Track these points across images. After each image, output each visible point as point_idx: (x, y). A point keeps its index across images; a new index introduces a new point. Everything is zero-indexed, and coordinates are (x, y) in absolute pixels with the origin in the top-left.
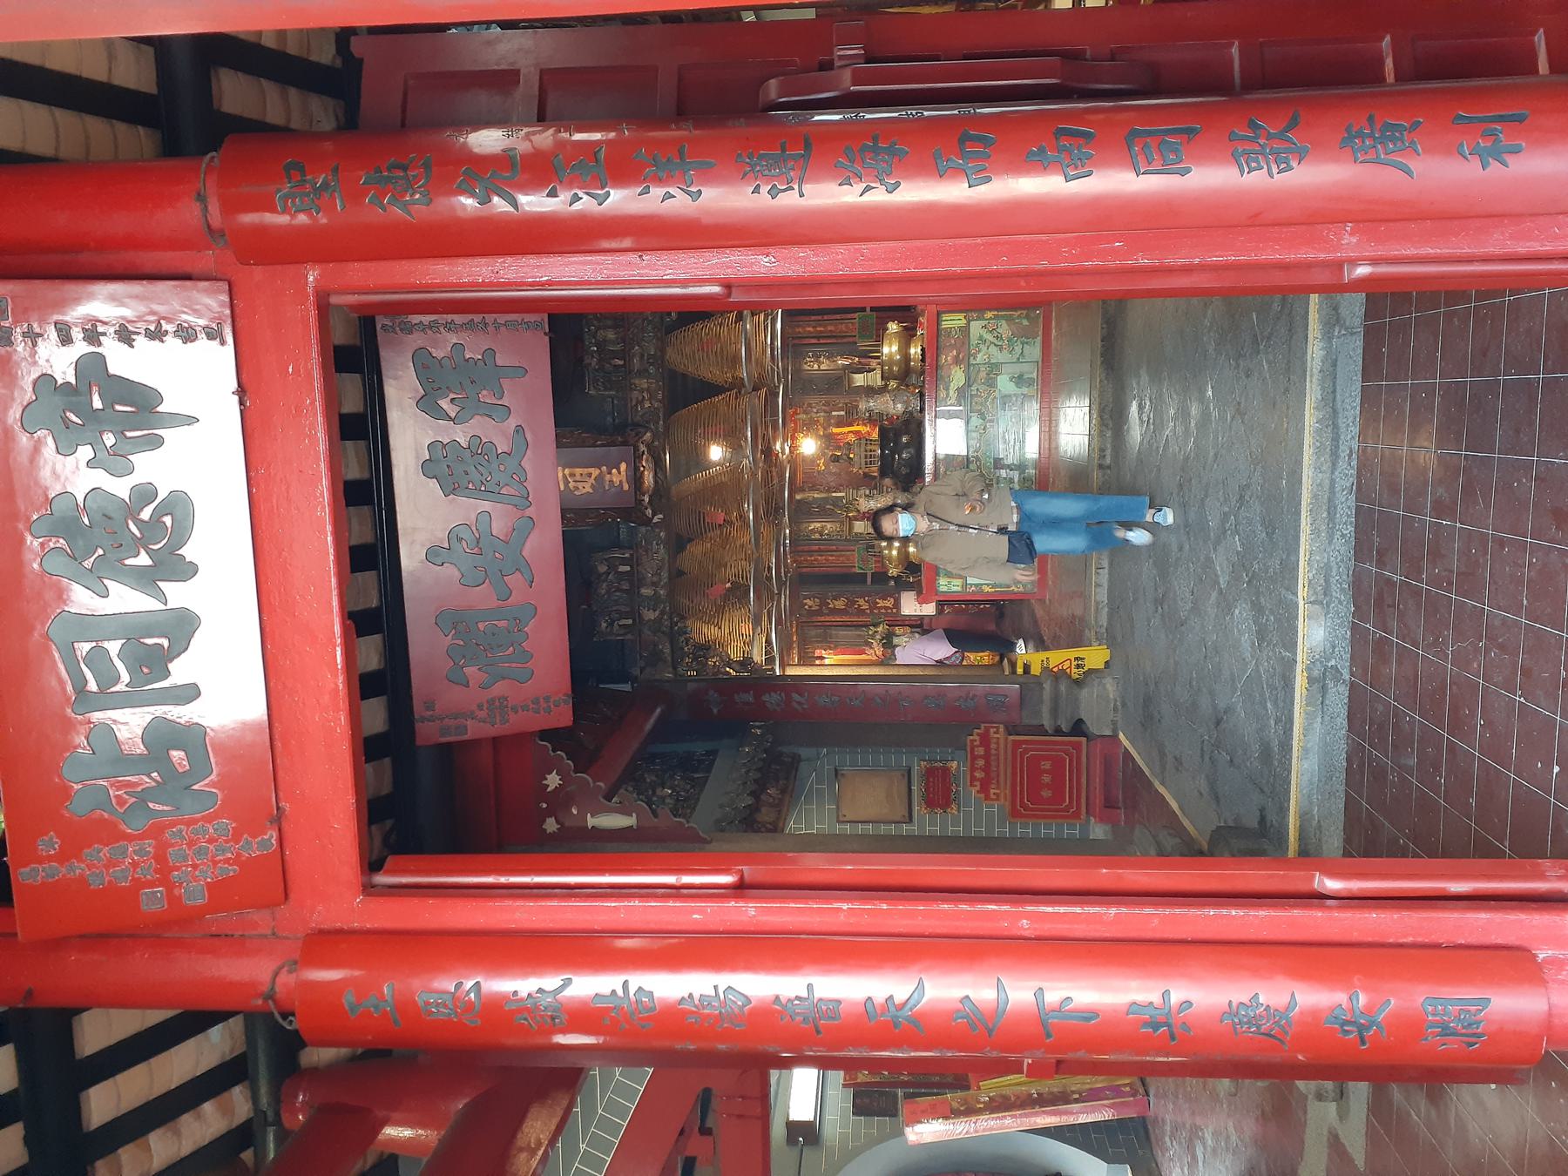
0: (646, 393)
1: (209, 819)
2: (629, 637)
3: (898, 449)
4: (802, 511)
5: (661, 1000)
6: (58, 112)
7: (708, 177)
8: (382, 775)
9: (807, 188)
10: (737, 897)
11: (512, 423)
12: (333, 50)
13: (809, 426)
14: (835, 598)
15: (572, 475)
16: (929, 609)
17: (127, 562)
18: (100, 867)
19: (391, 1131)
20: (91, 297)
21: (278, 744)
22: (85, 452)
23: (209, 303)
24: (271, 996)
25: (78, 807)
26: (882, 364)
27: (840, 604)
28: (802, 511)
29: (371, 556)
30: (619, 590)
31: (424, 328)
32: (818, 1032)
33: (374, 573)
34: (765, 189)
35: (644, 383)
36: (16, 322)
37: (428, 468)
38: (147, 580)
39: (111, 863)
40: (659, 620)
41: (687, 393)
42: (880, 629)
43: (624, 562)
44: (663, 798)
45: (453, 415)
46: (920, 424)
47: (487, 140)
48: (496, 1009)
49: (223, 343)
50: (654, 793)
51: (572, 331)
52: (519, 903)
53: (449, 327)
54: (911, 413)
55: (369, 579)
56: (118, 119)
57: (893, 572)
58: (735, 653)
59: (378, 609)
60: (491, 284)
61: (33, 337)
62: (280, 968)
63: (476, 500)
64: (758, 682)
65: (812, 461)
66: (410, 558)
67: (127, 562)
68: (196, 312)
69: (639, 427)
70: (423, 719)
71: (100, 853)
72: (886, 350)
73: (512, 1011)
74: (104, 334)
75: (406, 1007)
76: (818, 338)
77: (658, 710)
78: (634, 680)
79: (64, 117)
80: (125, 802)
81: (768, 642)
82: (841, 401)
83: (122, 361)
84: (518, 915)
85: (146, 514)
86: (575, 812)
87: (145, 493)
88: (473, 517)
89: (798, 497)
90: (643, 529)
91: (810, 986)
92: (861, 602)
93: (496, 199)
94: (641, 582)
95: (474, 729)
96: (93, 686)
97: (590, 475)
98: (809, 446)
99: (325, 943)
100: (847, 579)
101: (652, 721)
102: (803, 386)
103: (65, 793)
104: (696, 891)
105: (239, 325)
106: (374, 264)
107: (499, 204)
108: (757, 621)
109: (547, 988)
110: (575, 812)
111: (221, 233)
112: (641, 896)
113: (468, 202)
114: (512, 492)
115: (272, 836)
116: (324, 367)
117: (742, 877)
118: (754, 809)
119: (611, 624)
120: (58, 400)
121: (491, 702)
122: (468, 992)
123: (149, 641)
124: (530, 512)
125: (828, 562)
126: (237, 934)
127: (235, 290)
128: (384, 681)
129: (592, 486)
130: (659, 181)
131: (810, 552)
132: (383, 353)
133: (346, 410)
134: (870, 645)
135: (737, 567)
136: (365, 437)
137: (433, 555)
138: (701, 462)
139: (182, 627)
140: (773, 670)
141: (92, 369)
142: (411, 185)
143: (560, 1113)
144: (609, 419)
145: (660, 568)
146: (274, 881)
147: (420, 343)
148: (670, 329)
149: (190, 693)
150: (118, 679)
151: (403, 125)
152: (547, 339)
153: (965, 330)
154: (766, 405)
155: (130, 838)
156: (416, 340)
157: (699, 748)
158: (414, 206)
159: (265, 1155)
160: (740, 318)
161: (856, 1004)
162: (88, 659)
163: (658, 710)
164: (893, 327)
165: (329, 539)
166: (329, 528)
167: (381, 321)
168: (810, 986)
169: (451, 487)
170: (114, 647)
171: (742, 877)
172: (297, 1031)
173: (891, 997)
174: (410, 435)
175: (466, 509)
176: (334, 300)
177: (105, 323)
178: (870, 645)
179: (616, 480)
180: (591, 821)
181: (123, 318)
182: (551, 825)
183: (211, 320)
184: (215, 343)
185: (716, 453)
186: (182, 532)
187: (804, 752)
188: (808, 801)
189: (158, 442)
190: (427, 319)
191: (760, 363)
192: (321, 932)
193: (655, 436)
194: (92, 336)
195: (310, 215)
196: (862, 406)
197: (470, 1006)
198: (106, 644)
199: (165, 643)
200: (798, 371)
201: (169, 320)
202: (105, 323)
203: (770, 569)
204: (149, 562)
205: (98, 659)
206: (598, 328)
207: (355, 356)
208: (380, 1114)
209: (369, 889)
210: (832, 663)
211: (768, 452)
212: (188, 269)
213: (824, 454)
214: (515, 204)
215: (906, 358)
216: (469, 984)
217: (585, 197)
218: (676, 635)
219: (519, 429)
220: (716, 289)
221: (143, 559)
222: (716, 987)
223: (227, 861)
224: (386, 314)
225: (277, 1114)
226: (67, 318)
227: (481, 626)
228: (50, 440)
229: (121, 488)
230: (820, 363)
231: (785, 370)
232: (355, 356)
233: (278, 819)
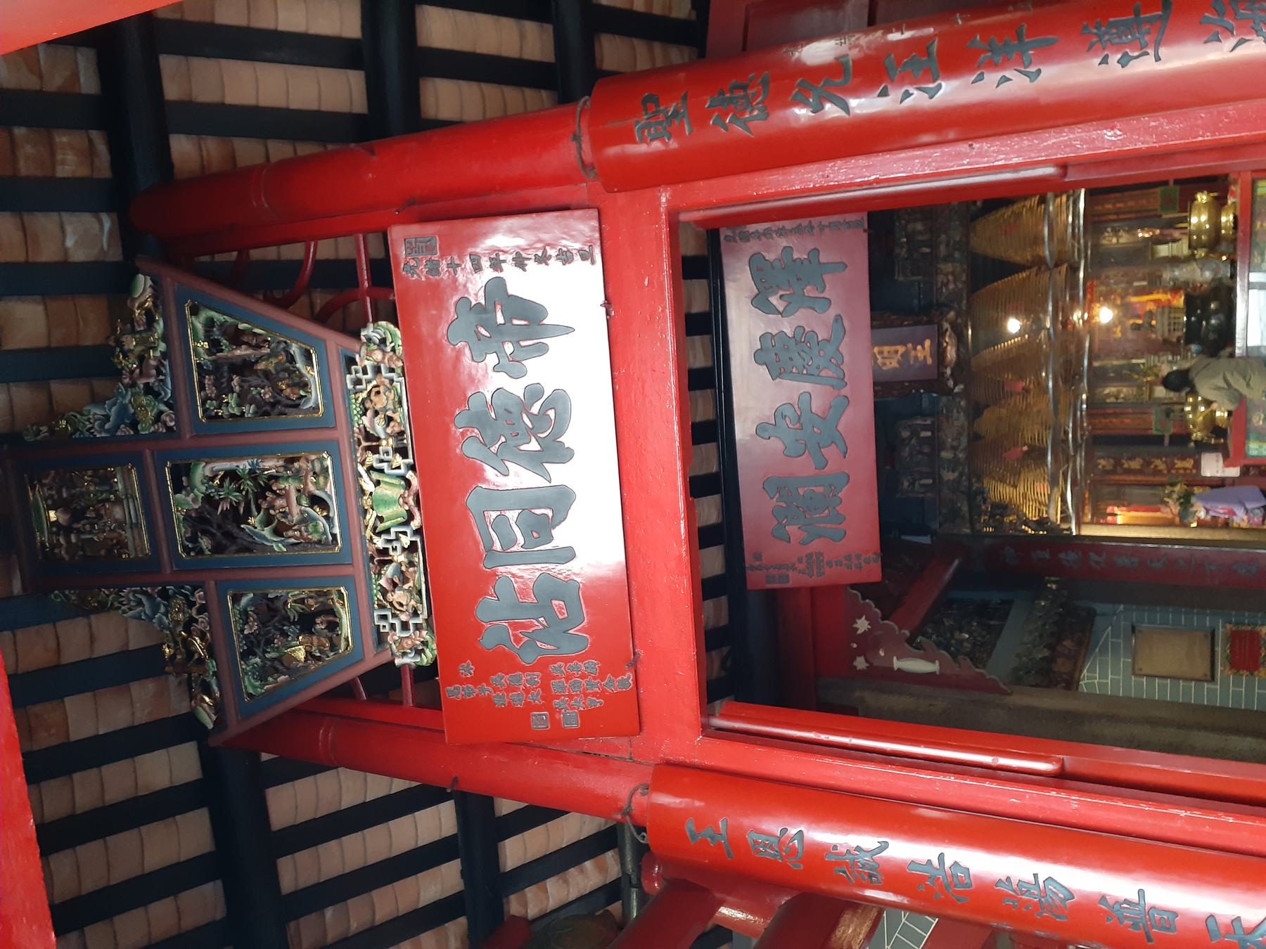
0: (950, 278)
1: (581, 658)
2: (929, 495)
3: (1207, 315)
4: (1099, 377)
5: (978, 878)
6: (485, 86)
7: (1049, 54)
8: (716, 611)
9: (1163, 51)
10: (1059, 788)
11: (832, 313)
12: (689, 6)
13: (1107, 298)
14: (1130, 459)
15: (881, 353)
16: (1234, 472)
17: (523, 447)
18: (505, 691)
19: (725, 911)
20: (495, 231)
21: (634, 599)
22: (492, 359)
23: (579, 230)
24: (628, 813)
25: (488, 641)
26: (1190, 235)
27: (1135, 464)
28: (1099, 377)
29: (710, 429)
30: (920, 452)
31: (758, 235)
32: (1149, 940)
33: (714, 444)
34: (1114, 58)
35: (948, 267)
36: (443, 256)
37: (759, 357)
38: (536, 462)
39: (510, 689)
40: (958, 481)
41: (991, 276)
42: (1177, 488)
43: (925, 428)
44: (961, 642)
45: (781, 309)
46: (1231, 291)
47: (818, 52)
48: (817, 854)
49: (593, 262)
50: (952, 636)
51: (892, 229)
52: (839, 762)
53: (781, 232)
54: (1220, 279)
55: (710, 450)
56: (527, 86)
57: (1197, 435)
58: (1032, 515)
59: (716, 475)
60: (821, 188)
61: (453, 266)
62: (635, 790)
63: (800, 373)
64: (1057, 541)
65: (1108, 329)
66: (743, 430)
67: (523, 447)
68: (573, 238)
69: (943, 307)
70: (753, 568)
71: (501, 679)
72: (1194, 220)
73: (831, 863)
74: (504, 261)
75: (738, 841)
77: (956, 562)
78: (933, 533)
79: (491, 90)
80: (521, 639)
81: (1064, 501)
82: (1141, 271)
83: (520, 283)
84: (837, 773)
85: (535, 409)
86: (882, 653)
87: (534, 392)
88: (796, 397)
89: (1096, 364)
90: (944, 399)
91: (1141, 893)
92: (1158, 462)
93: (828, 106)
94: (942, 446)
95: (795, 579)
96: (498, 546)
97: (897, 352)
99: (672, 773)
100: (1145, 441)
101: (951, 570)
102: (1100, 260)
103: (478, 629)
104: (1013, 773)
105: (607, 245)
106: (713, 182)
107: (831, 111)
108: (1054, 482)
109: (864, 846)
110: (882, 653)
111: (592, 166)
112: (955, 773)
113: (802, 113)
114: (830, 374)
115: (629, 677)
116: (673, 277)
117: (1063, 766)
118: (1050, 660)
119: (912, 484)
120: (473, 318)
121: (809, 556)
122: (792, 839)
123: (538, 512)
124: (845, 391)
125: (1128, 424)
126: (603, 754)
127: (603, 216)
128: (720, 534)
129: (899, 362)
130: (992, 65)
131: (1105, 415)
132: (725, 260)
133: (695, 310)
134: (1166, 504)
135: (1032, 431)
136: (709, 332)
137: (762, 430)
138: (1002, 336)
139: (562, 500)
140: (1070, 529)
141: (497, 289)
142: (750, 104)
143: (869, 923)
144: (916, 301)
145: (960, 434)
146: (628, 715)
147: (756, 249)
148: (974, 217)
149: (568, 554)
150: (515, 542)
151: (744, 49)
152: (865, 236)
154: (1063, 277)
155: (524, 669)
156: (753, 247)
157: (995, 597)
158: (752, 122)
159: (630, 912)
160: (1043, 201)
161: (1196, 919)
162: (495, 525)
163: (956, 562)
164: (1202, 198)
165: (676, 427)
166: (675, 419)
167: (724, 232)
168: (1141, 893)
169: (778, 372)
170: (512, 515)
171: (1063, 766)
172: (647, 845)
173: (1238, 919)
174: (745, 326)
175: (790, 390)
176: (683, 217)
177: (505, 252)
178: (1166, 504)
179: (920, 355)
180: (897, 664)
181: (518, 247)
182: (860, 663)
183: (584, 244)
184: (588, 263)
185: (1013, 325)
186: (561, 424)
187: (1100, 607)
188: (1104, 651)
189: (542, 350)
190: (761, 227)
191: (1062, 241)
192: (669, 763)
193: (958, 315)
194: (496, 265)
195: (662, 140)
196: (1167, 275)
197: (794, 852)
198: (508, 514)
199: (550, 513)
200: (1096, 246)
201: (552, 246)
202: (505, 252)
203: (1066, 433)
204: (538, 448)
205: (502, 521)
206: (908, 222)
207: (701, 266)
208: (718, 895)
209: (708, 731)
210: (1124, 523)
211: (1066, 322)
212: (565, 200)
213: (1121, 323)
214: (846, 108)
215: (1217, 226)
216: (793, 831)
217: (916, 93)
218: (975, 496)
219: (838, 318)
220: (1050, 170)
221: (534, 446)
222: (1035, 876)
223: (594, 694)
224: (728, 227)
225: (639, 879)
226: (478, 250)
227: (801, 491)
228: (467, 351)
229: (517, 388)
231: (1086, 244)
232: (701, 266)
233: (634, 665)
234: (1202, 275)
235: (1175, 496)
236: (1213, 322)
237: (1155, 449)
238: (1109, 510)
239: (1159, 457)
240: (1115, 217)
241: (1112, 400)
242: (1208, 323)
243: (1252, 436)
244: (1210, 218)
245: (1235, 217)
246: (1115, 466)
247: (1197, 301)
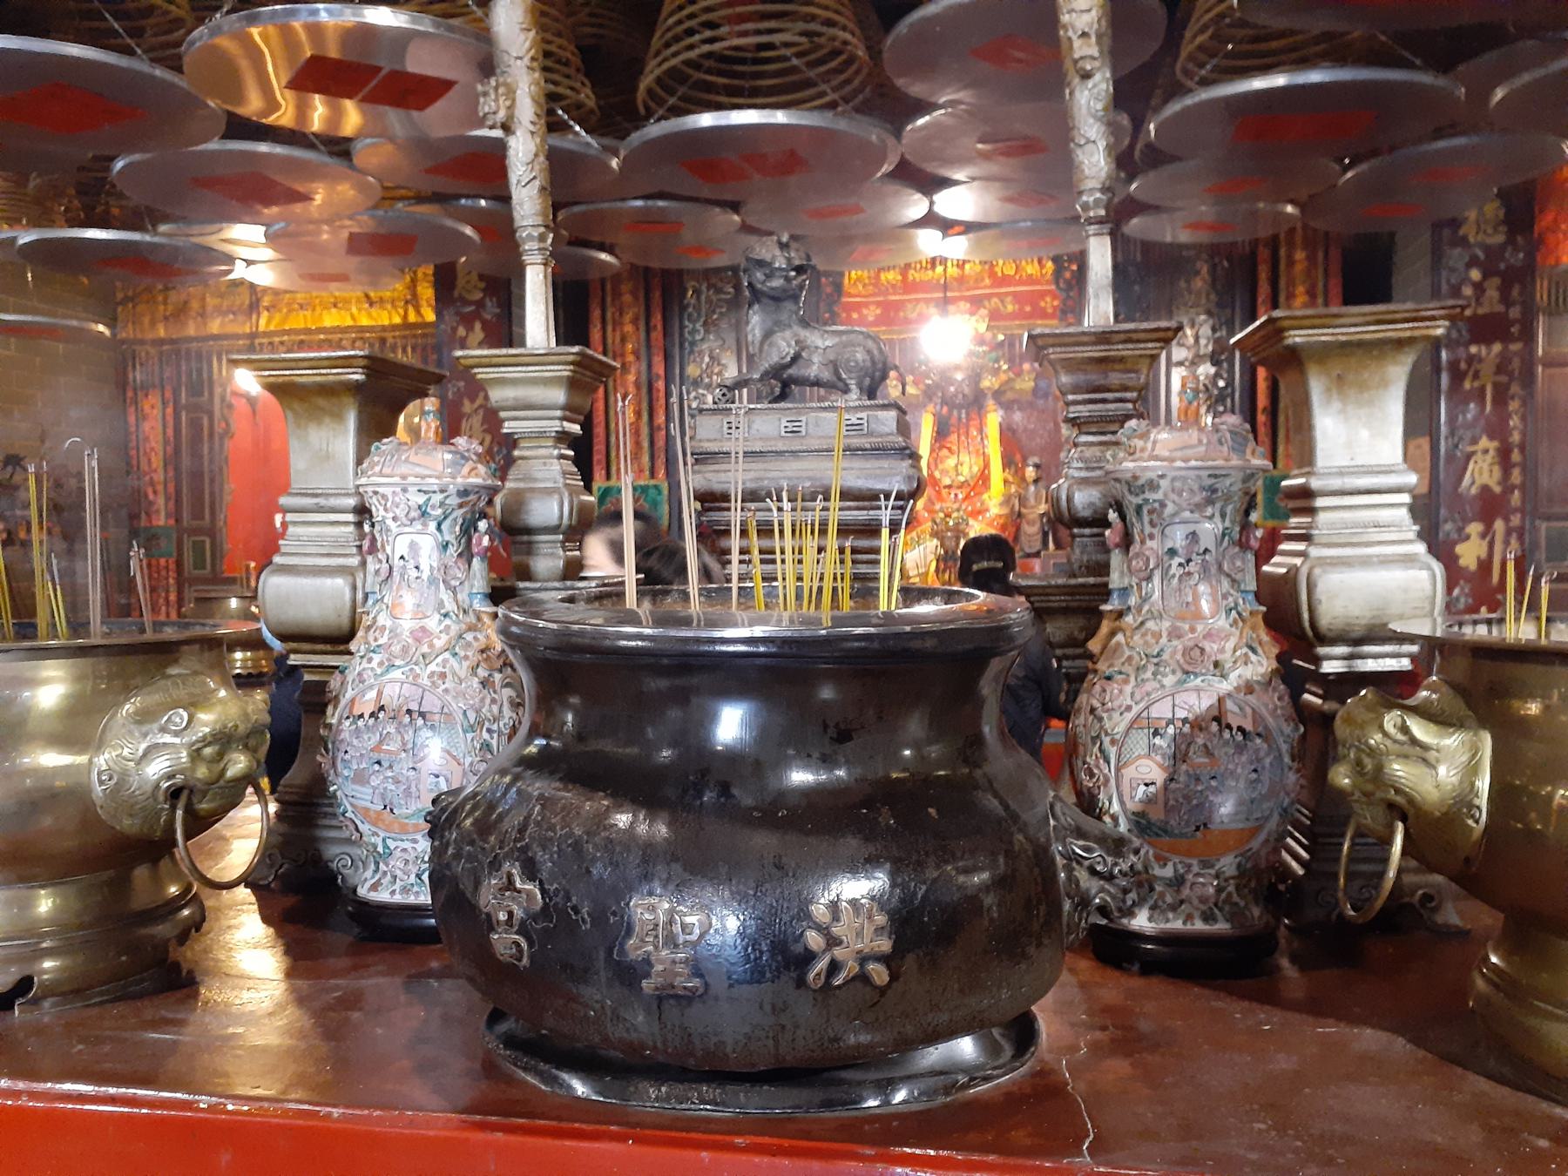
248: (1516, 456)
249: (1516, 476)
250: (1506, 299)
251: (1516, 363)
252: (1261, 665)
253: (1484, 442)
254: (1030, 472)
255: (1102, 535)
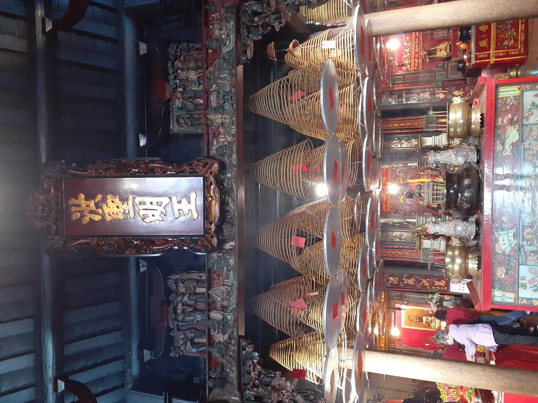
14: (408, 278)
40: (227, 343)
54: (470, 163)
65: (396, 197)
76: (401, 129)
92: (424, 281)
98: (394, 189)
153: (520, 99)
215: (468, 122)
230: (401, 144)
234: (456, 159)
235: (434, 301)
236: (466, 194)
237: (422, 272)
238: (397, 306)
239: (425, 278)
240: (399, 131)
241: (398, 240)
242: (462, 195)
243: (497, 285)
244: (463, 115)
245: (482, 115)
246: (399, 282)
247: (453, 179)
248: (424, 90)
249: (427, 90)
250: (395, 94)
251: (407, 92)
252: (451, 151)
253: (421, 95)
254: (422, 173)
255: (444, 260)
